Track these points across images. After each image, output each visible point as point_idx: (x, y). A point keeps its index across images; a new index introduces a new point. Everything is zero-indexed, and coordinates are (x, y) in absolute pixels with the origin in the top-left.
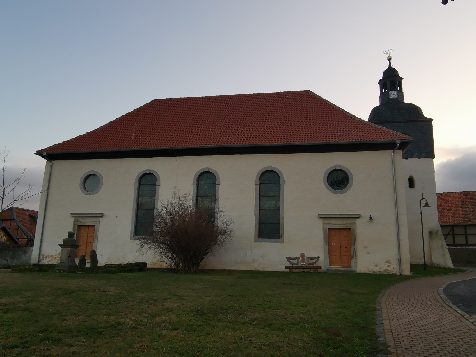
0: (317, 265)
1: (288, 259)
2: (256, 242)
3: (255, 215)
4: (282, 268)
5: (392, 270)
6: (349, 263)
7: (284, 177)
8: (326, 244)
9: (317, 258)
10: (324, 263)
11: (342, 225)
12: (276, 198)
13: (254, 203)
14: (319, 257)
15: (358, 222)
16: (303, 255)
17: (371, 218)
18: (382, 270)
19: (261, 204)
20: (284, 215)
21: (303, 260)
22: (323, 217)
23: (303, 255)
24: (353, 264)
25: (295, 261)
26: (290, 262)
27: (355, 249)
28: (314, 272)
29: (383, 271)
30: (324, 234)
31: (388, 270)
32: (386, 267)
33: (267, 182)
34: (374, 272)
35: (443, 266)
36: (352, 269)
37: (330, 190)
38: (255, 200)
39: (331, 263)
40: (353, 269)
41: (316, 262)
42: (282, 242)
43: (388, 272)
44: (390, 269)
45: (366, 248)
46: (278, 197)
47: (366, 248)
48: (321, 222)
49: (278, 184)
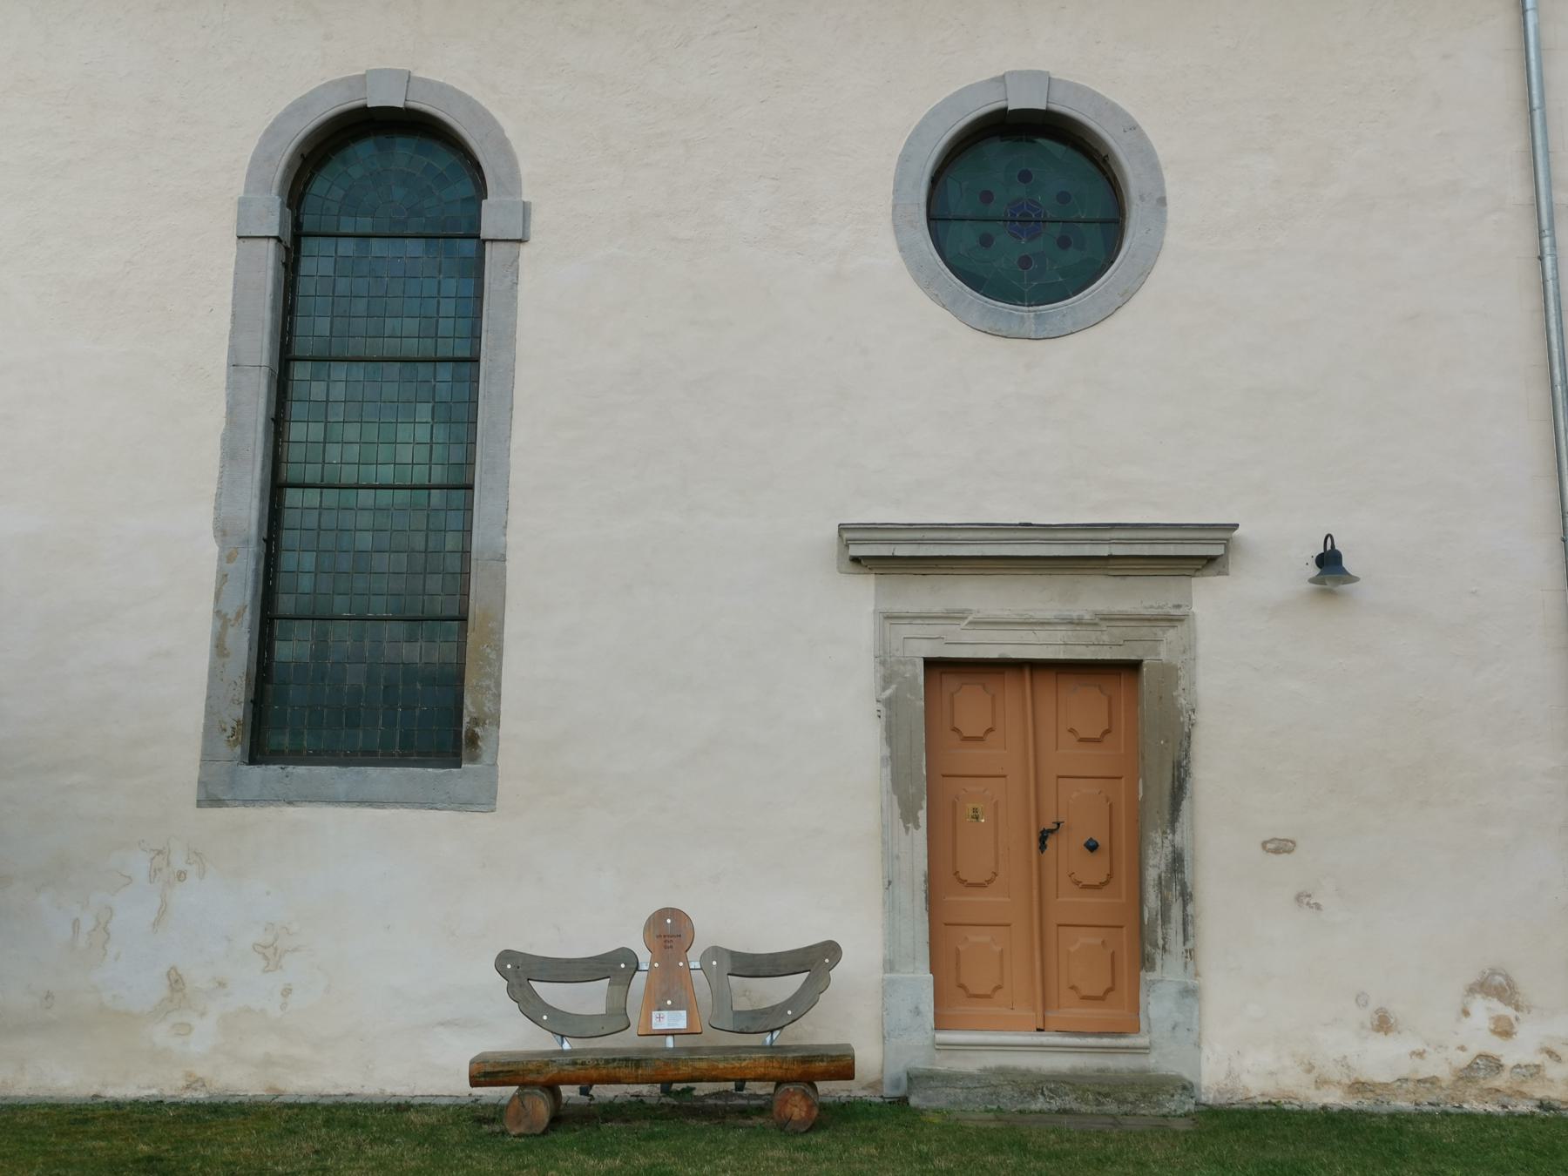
0: (817, 1030)
1: (521, 972)
2: (209, 799)
3: (222, 532)
4: (436, 1070)
5: (1535, 1071)
6: (1116, 996)
7: (525, 168)
8: (908, 817)
9: (816, 961)
10: (877, 1020)
11: (1060, 634)
12: (445, 372)
13: (212, 418)
14: (829, 952)
15: (1206, 598)
16: (669, 930)
17: (1329, 561)
18: (1440, 1066)
19: (296, 431)
20: (512, 539)
21: (670, 989)
22: (880, 556)
23: (669, 930)
24: (1158, 1006)
25: (588, 998)
26: (533, 1009)
27: (1177, 861)
28: (592, 1082)
29: (1444, 1073)
30: (891, 709)
31: (1496, 1066)
33: (365, 224)
34: (1359, 1087)
35: (381, 1101)
37: (951, 305)
38: (233, 389)
39: (953, 997)
40: (1164, 1061)
41: (802, 1003)
42: (483, 800)
43: (1500, 1082)
44: (1514, 1053)
45: (1280, 847)
46: (451, 369)
47: (1280, 847)
48: (865, 587)
49: (468, 246)
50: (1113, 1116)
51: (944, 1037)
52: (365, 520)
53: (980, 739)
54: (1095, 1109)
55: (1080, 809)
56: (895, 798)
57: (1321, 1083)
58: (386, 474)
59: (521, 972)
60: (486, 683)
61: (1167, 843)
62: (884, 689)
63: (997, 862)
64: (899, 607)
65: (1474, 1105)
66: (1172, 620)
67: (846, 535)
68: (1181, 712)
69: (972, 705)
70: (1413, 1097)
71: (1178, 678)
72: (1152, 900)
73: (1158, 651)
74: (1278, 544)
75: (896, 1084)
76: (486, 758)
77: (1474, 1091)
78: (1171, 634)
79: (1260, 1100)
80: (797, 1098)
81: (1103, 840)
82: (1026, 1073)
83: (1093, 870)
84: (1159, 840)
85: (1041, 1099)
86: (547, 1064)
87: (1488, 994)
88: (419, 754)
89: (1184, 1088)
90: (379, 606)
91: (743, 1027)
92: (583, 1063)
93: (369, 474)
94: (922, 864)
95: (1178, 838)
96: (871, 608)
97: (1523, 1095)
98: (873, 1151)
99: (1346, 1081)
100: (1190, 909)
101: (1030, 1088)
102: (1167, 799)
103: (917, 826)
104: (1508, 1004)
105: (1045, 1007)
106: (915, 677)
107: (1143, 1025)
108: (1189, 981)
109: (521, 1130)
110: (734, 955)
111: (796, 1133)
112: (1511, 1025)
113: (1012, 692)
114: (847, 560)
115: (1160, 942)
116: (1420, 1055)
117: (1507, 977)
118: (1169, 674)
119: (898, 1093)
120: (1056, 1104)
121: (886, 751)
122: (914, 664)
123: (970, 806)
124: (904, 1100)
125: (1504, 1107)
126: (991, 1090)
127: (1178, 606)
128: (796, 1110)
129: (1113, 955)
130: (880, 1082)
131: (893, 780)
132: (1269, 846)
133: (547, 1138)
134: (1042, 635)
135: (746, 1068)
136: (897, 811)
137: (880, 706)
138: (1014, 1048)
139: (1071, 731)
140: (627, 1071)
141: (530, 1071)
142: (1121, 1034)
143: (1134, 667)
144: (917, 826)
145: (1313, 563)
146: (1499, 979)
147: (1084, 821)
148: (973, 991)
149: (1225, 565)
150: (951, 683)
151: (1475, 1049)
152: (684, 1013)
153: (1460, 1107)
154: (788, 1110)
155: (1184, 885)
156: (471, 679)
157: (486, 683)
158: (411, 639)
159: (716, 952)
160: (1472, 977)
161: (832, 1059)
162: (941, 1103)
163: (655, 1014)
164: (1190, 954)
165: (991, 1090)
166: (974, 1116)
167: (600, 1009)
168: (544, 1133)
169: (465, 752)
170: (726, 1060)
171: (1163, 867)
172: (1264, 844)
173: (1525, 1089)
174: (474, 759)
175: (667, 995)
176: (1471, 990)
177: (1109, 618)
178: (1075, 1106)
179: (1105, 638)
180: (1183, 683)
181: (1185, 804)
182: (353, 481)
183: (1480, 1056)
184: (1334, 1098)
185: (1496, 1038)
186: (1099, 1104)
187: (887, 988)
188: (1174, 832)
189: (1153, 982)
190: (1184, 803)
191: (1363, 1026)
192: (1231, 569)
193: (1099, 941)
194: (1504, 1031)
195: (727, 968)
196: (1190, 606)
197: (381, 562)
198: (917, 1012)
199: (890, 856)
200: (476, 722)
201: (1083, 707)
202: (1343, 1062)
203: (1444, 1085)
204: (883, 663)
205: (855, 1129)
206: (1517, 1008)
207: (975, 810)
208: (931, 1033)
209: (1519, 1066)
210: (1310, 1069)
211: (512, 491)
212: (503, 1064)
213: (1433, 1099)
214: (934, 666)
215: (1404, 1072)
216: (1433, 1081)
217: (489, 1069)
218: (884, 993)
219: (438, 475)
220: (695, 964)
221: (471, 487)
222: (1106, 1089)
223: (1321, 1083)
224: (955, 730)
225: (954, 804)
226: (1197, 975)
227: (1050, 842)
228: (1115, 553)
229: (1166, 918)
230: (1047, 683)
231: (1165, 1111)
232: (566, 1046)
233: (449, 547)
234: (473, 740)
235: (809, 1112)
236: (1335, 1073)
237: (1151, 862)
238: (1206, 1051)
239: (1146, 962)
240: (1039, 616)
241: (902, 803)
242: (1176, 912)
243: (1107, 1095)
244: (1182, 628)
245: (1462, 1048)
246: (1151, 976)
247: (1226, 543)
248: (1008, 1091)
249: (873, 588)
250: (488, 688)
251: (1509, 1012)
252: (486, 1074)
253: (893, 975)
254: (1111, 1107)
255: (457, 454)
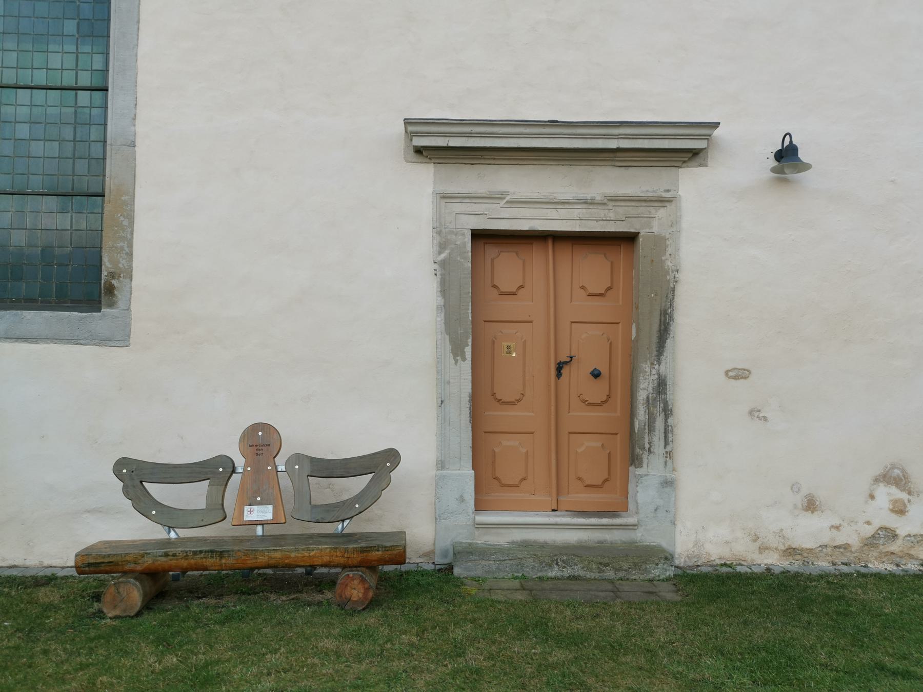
0: (379, 521)
1: (135, 476)
8: (457, 352)
9: (381, 464)
10: (427, 509)
11: (577, 212)
14: (391, 457)
15: (689, 183)
16: (261, 440)
17: (787, 155)
18: (851, 536)
22: (441, 147)
23: (261, 440)
24: (644, 491)
25: (192, 496)
26: (144, 504)
27: (661, 385)
30: (445, 269)
31: (892, 535)
32: (879, 513)
34: (791, 552)
36: (638, 536)
39: (489, 488)
40: (649, 535)
41: (368, 498)
42: (119, 338)
43: (895, 547)
44: (904, 527)
45: (739, 375)
47: (739, 375)
50: (611, 581)
51: (483, 518)
52: (23, 112)
53: (516, 486)
54: (597, 575)
55: (588, 345)
56: (447, 337)
57: (763, 549)
58: (40, 78)
59: (135, 476)
60: (120, 244)
61: (654, 371)
62: (440, 253)
63: (524, 385)
64: (452, 189)
65: (876, 566)
66: (663, 201)
67: (410, 129)
68: (667, 273)
69: (507, 266)
70: (830, 559)
71: (666, 246)
72: (642, 414)
73: (652, 225)
74: (746, 143)
75: (445, 554)
76: (121, 304)
77: (875, 554)
78: (662, 213)
79: (718, 562)
80: (356, 582)
81: (604, 370)
82: (543, 546)
83: (597, 390)
84: (648, 370)
85: (556, 568)
86: (143, 556)
87: (888, 483)
88: (73, 301)
89: (666, 559)
90: (36, 183)
91: (319, 518)
92: (174, 555)
93: (25, 77)
94: (468, 388)
95: (662, 368)
96: (430, 190)
97: (911, 556)
98: (415, 639)
99: (782, 547)
100: (670, 421)
101: (547, 559)
102: (655, 339)
103: (464, 359)
104: (904, 490)
105: (558, 493)
106: (465, 244)
107: (631, 506)
108: (668, 475)
109: (117, 612)
110: (312, 460)
111: (354, 612)
112: (905, 505)
113: (538, 260)
114: (412, 149)
115: (647, 446)
116: (837, 528)
117: (903, 471)
118: (660, 242)
119: (446, 561)
120: (567, 572)
121: (441, 301)
122: (464, 234)
123: (505, 344)
124: (450, 568)
125: (898, 565)
126: (517, 561)
127: (668, 191)
128: (355, 592)
129: (609, 454)
130: (433, 552)
131: (445, 323)
132: (731, 374)
133: (140, 619)
134: (563, 212)
135: (314, 556)
136: (449, 347)
137: (436, 266)
138: (536, 525)
139: (583, 288)
140: (212, 561)
141: (128, 562)
142: (613, 514)
143: (630, 239)
144: (464, 359)
145: (772, 157)
146: (897, 472)
147: (591, 356)
148: (504, 482)
149: (706, 159)
150: (491, 251)
151: (877, 524)
152: (270, 507)
153: (866, 566)
154: (348, 593)
155: (666, 403)
156: (107, 243)
157: (120, 244)
158: (63, 211)
159: (298, 458)
160: (878, 471)
161: (386, 549)
162: (479, 572)
163: (247, 508)
164: (669, 455)
165: (517, 561)
166: (504, 585)
167: (201, 504)
168: (139, 614)
169: (104, 300)
170: (297, 550)
171: (650, 390)
172: (727, 373)
173: (912, 552)
174: (111, 305)
175: (257, 493)
176: (877, 480)
177: (614, 199)
178: (582, 573)
179: (612, 215)
180: (669, 250)
181: (669, 342)
182: (12, 82)
183: (881, 528)
184: (773, 560)
185: (893, 515)
186: (601, 571)
187: (439, 482)
188: (659, 364)
189: (641, 476)
190: (668, 341)
191: (795, 507)
192: (709, 163)
193: (599, 444)
194: (900, 510)
195: (307, 471)
196: (677, 190)
197: (37, 148)
198: (462, 499)
199: (443, 382)
200: (112, 275)
201: (592, 269)
202: (781, 534)
203: (853, 550)
204: (439, 233)
205: (404, 606)
206: (910, 493)
207: (509, 347)
208: (472, 516)
209: (909, 536)
210: (756, 539)
211: (140, 90)
212: (104, 557)
213: (845, 560)
214: (479, 236)
215: (825, 540)
216: (846, 547)
217: (92, 561)
218: (437, 484)
219: (85, 79)
220: (281, 468)
221: (106, 90)
222: (606, 560)
223: (763, 549)
224: (495, 286)
225: (493, 343)
226: (674, 470)
227: (565, 371)
228: (622, 146)
229: (651, 429)
230: (565, 253)
231: (651, 576)
232: (173, 535)
233: (93, 138)
234: (110, 290)
235: (365, 593)
236: (774, 542)
237: (642, 386)
238: (679, 527)
239: (634, 460)
240: (562, 197)
241: (452, 341)
242: (659, 424)
243: (606, 565)
244: (670, 207)
245: (868, 523)
246: (639, 471)
247: (708, 137)
248: (530, 562)
249: (432, 175)
250: (122, 248)
251: (904, 496)
252: (89, 565)
253: (444, 472)
254: (610, 574)
255: (98, 63)
